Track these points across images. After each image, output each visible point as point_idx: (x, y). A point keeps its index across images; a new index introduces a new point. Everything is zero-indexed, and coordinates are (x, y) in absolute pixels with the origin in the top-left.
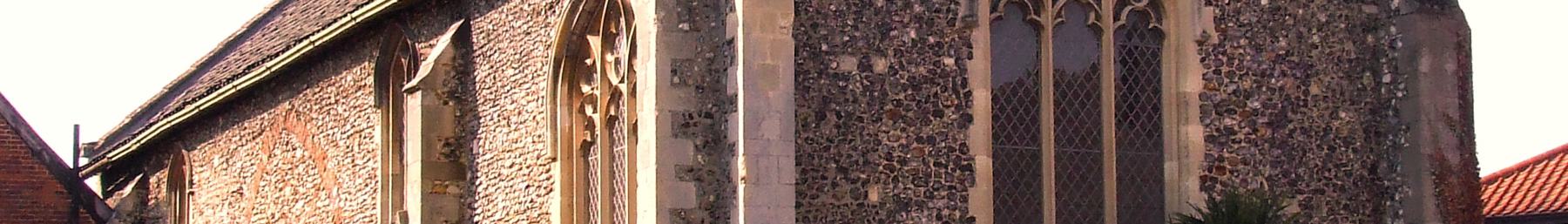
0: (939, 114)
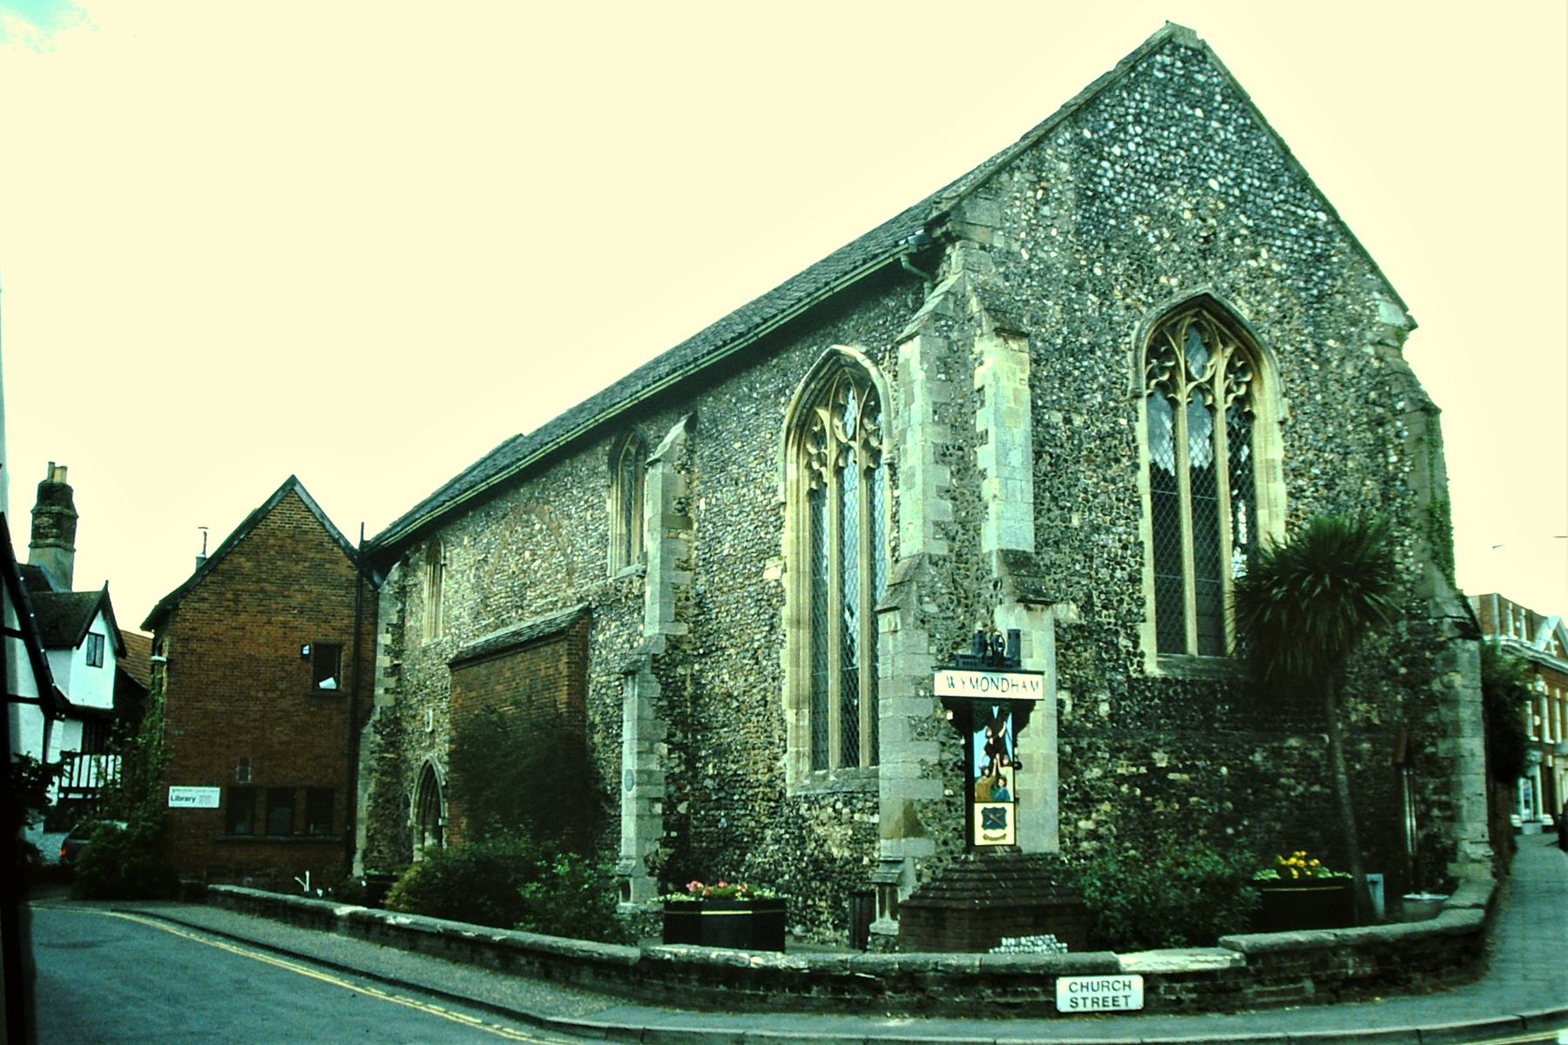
0: (1117, 461)
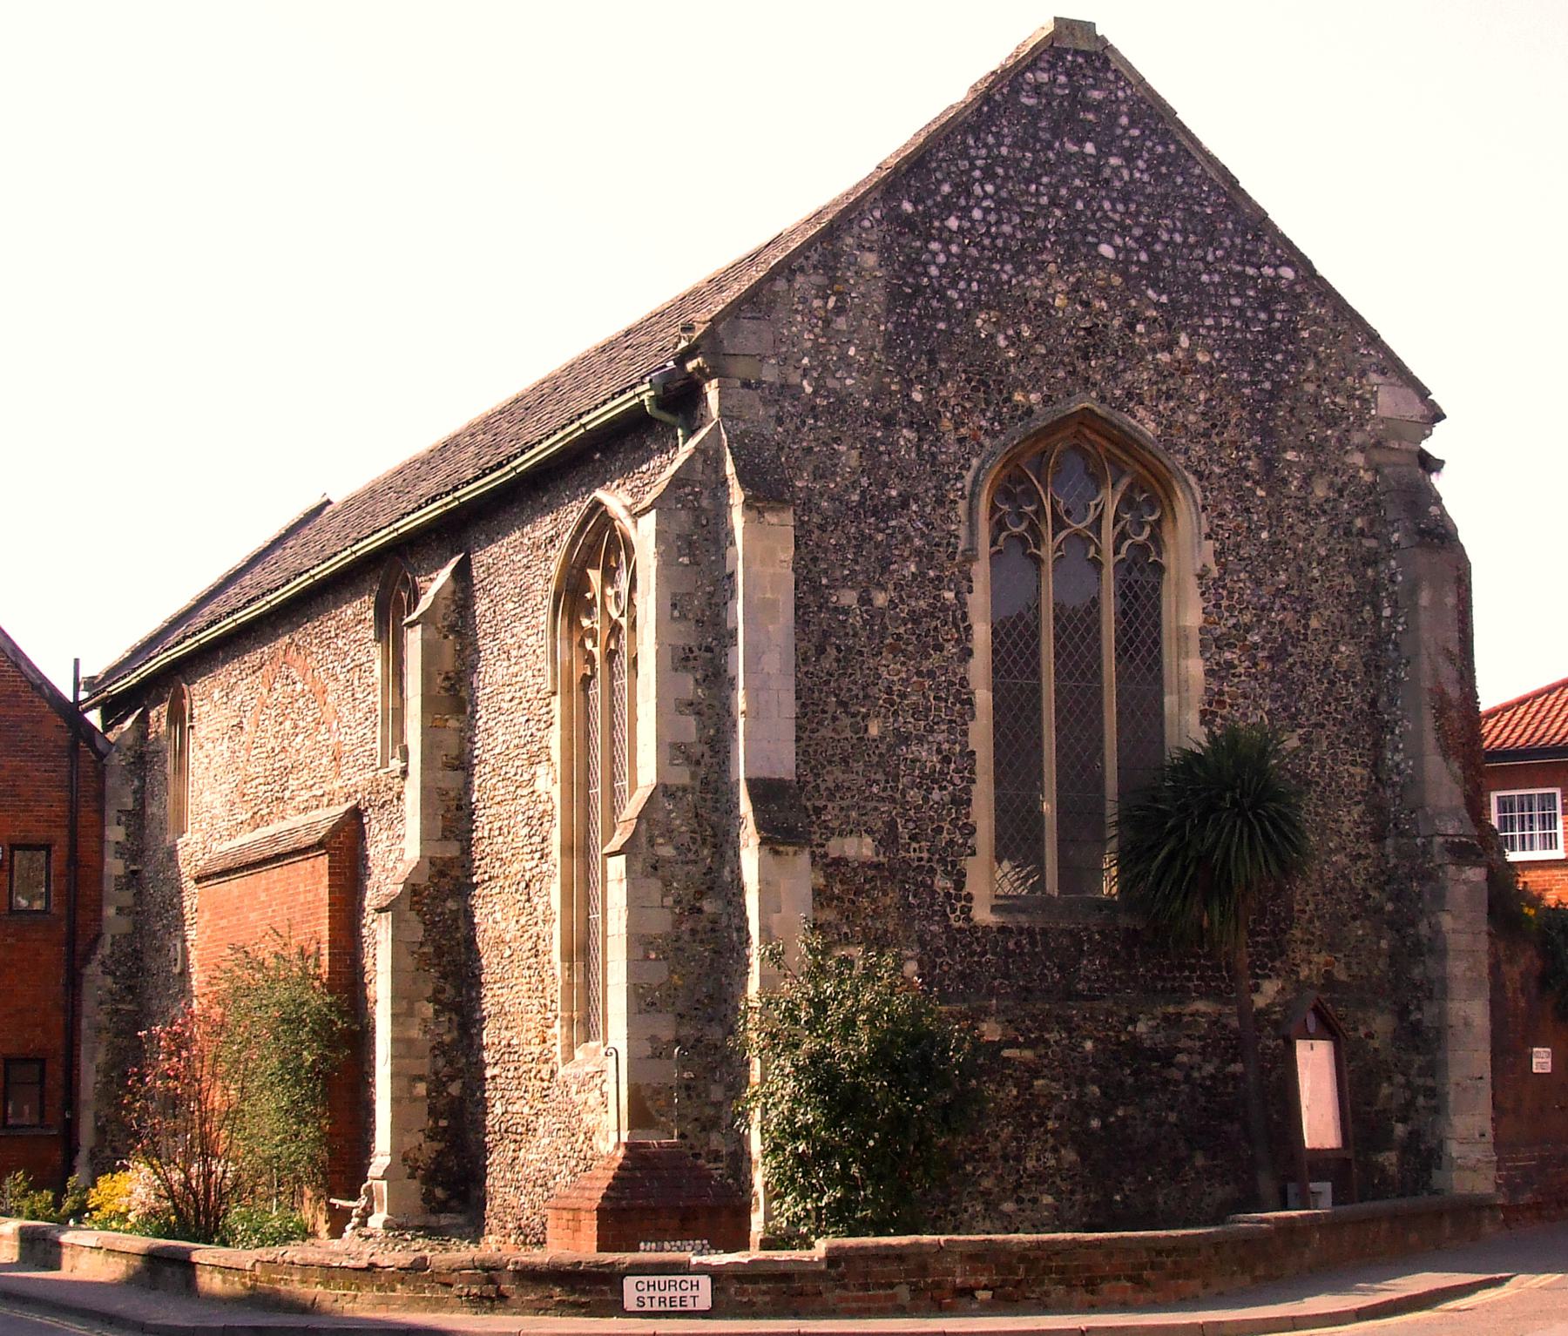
0: (939, 648)
